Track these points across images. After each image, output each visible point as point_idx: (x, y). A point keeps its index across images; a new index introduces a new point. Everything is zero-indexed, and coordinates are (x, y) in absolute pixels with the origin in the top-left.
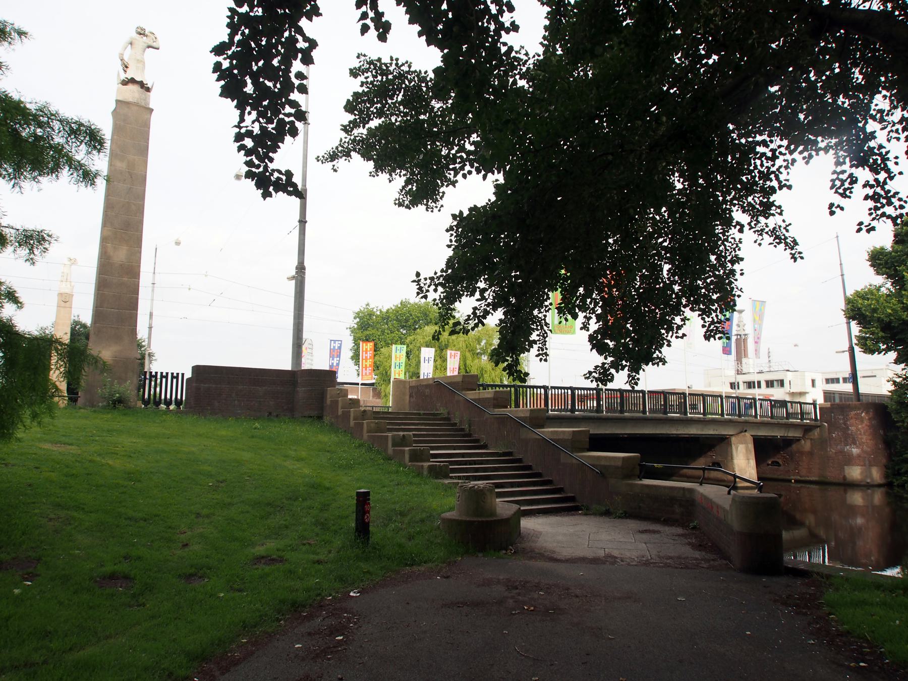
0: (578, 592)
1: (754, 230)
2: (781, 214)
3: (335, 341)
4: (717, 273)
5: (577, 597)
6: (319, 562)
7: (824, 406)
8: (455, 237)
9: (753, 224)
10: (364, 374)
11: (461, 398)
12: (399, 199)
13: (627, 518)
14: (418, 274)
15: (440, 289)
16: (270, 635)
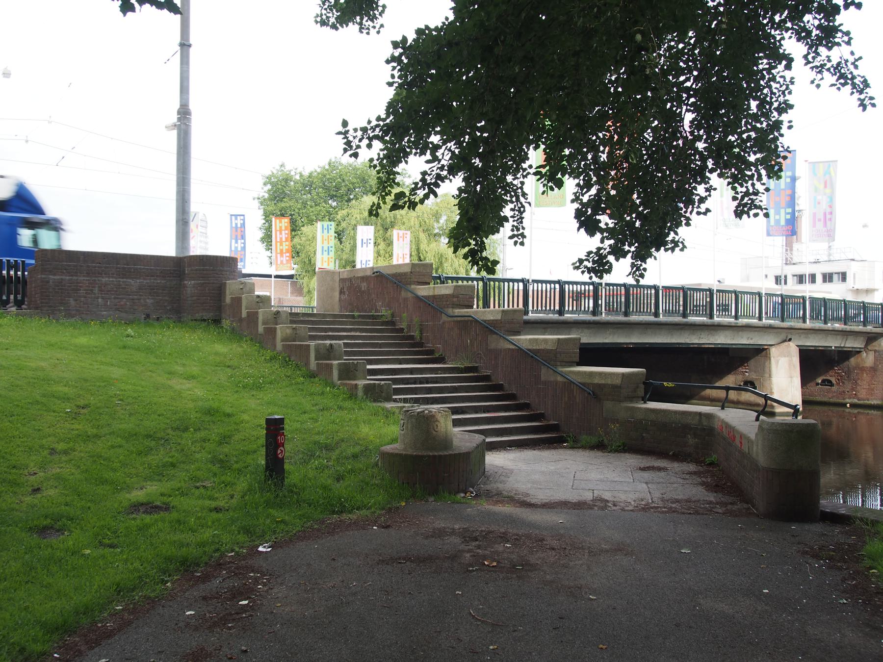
0: (555, 543)
1: (811, 65)
2: (848, 43)
3: (236, 216)
4: (758, 125)
5: (553, 549)
6: (217, 510)
8: (399, 70)
10: (279, 263)
12: (322, 15)
14: (345, 124)
15: (377, 145)
16: (153, 601)
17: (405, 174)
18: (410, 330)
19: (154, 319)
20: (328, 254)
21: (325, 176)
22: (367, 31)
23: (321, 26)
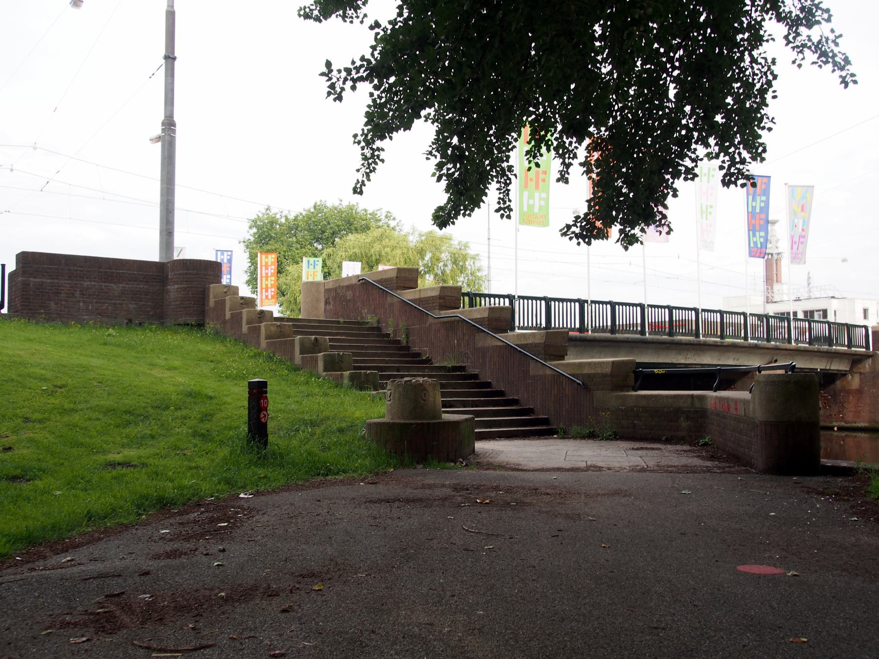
1: (791, 45)
2: (828, 20)
3: (223, 252)
9: (791, 38)
11: (395, 300)
13: (617, 439)
14: (328, 64)
17: (390, 217)
18: (396, 335)
19: (136, 324)
20: (314, 268)
21: (310, 219)
22: (351, 19)
23: (305, 19)
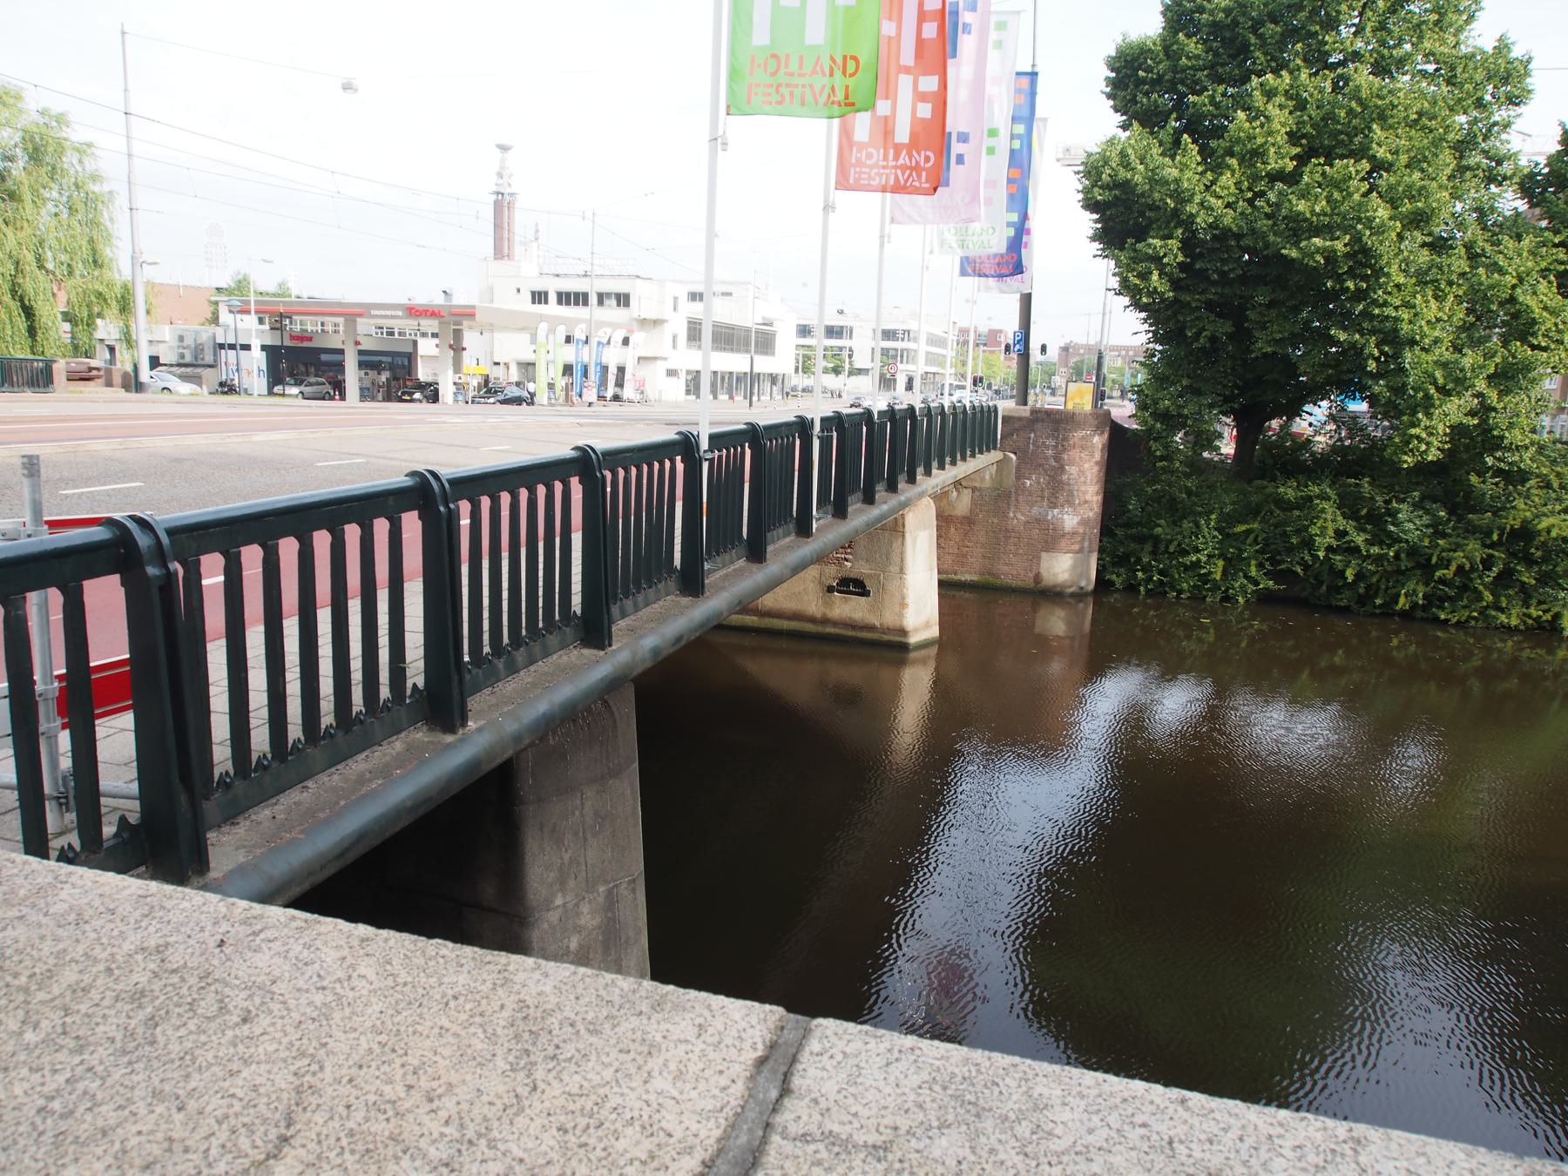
7: (1015, 415)
